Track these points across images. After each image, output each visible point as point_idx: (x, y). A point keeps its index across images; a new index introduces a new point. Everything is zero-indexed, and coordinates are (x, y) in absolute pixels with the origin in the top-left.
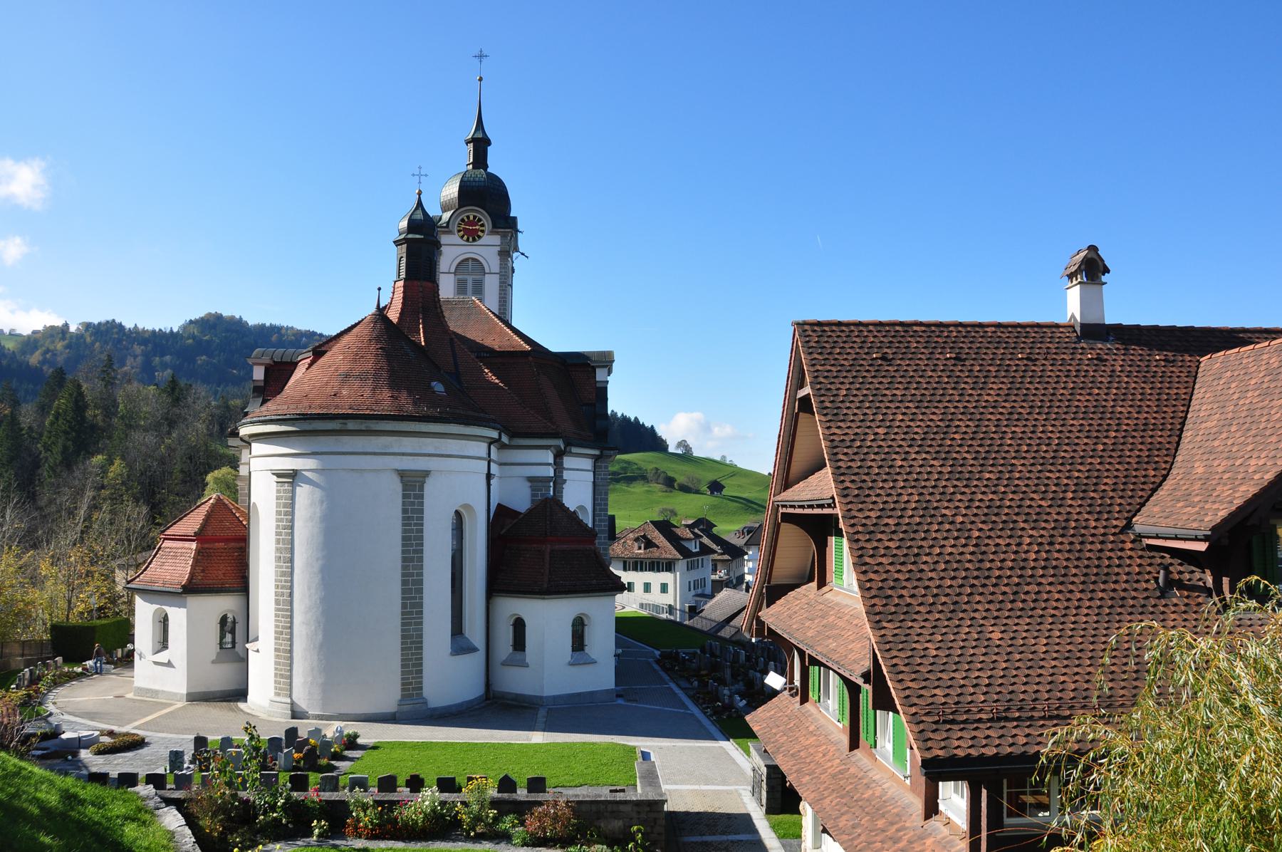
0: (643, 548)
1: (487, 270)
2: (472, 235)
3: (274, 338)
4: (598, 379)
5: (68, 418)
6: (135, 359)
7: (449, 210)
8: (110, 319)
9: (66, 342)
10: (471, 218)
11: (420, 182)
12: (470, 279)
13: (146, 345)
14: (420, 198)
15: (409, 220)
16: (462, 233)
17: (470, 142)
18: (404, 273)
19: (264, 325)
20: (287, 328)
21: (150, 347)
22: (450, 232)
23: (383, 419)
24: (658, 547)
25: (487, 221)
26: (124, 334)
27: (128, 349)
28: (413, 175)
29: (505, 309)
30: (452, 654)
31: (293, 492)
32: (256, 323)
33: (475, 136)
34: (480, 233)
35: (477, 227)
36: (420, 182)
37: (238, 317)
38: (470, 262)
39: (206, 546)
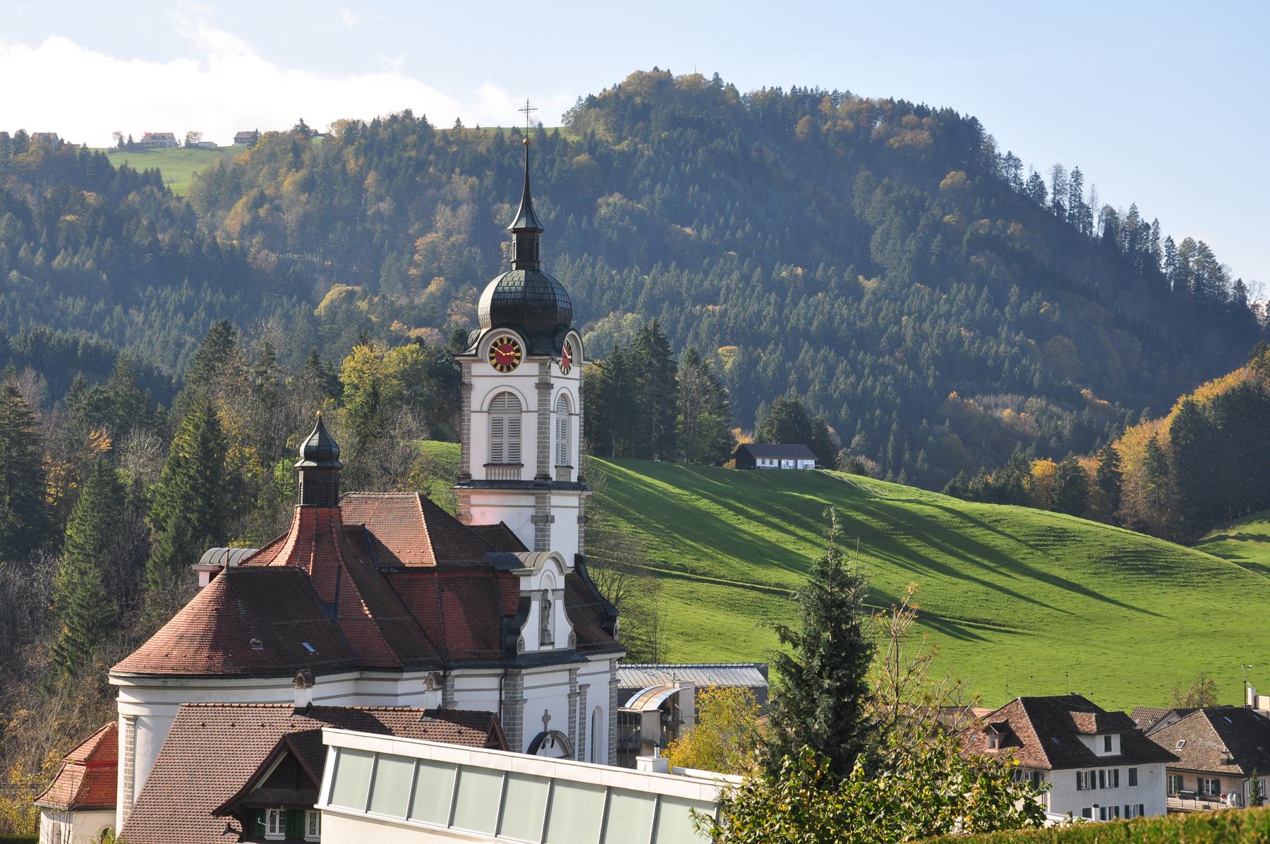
0: (997, 746)
1: (524, 408)
2: (506, 364)
3: (802, 126)
4: (522, 588)
5: (192, 472)
6: (454, 210)
8: (398, 110)
9: (303, 173)
12: (506, 418)
13: (480, 176)
19: (775, 94)
20: (835, 98)
21: (490, 175)
22: (481, 361)
23: (193, 678)
24: (1021, 745)
26: (431, 148)
27: (439, 187)
31: (135, 732)
32: (757, 88)
33: (517, 227)
34: (515, 361)
35: (512, 353)
37: (709, 77)
38: (507, 394)
39: (94, 770)
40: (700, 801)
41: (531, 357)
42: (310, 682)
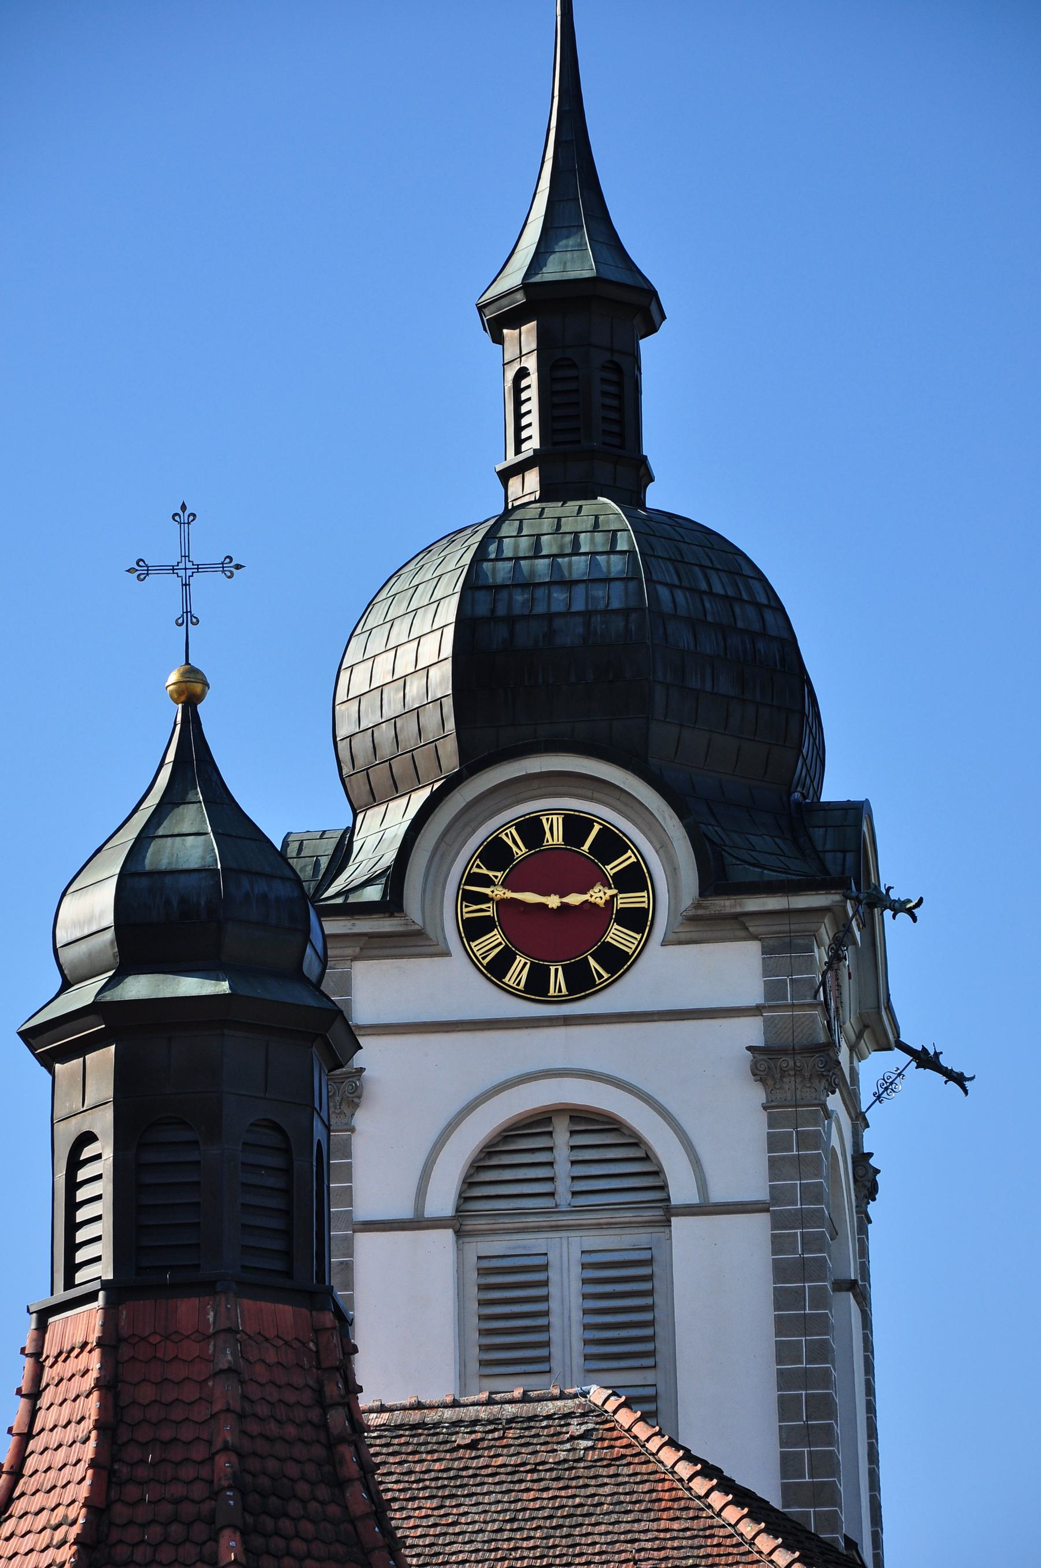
7: (396, 789)
10: (555, 836)
11: (188, 618)
14: (191, 724)
15: (123, 877)
16: (495, 938)
17: (514, 318)
18: (104, 1249)
25: (663, 847)
28: (142, 570)
29: (827, 1464)
30: (98, 1140)
33: (551, 272)
34: (617, 935)
35: (598, 895)
36: (188, 618)
38: (562, 1137)
40: (541, 773)
41: (727, 905)
42: (472, 1440)
